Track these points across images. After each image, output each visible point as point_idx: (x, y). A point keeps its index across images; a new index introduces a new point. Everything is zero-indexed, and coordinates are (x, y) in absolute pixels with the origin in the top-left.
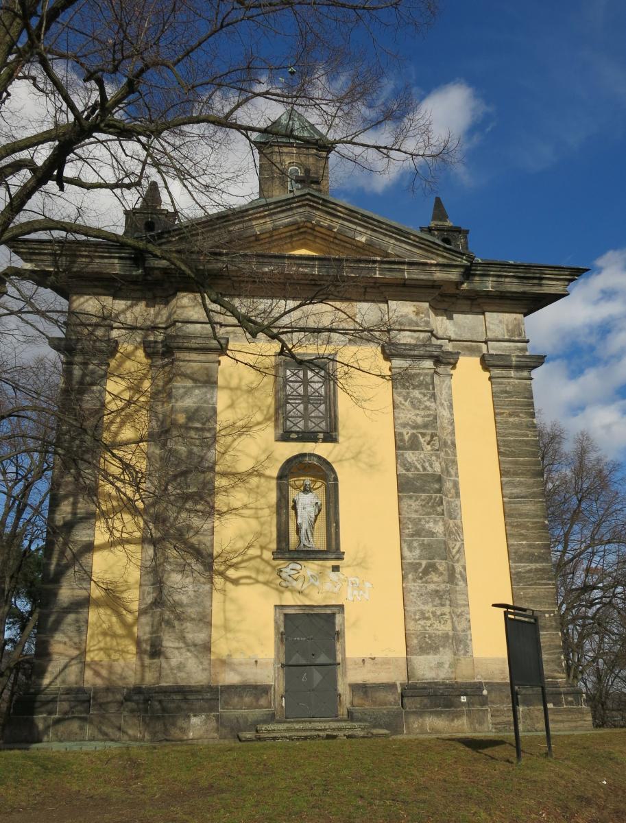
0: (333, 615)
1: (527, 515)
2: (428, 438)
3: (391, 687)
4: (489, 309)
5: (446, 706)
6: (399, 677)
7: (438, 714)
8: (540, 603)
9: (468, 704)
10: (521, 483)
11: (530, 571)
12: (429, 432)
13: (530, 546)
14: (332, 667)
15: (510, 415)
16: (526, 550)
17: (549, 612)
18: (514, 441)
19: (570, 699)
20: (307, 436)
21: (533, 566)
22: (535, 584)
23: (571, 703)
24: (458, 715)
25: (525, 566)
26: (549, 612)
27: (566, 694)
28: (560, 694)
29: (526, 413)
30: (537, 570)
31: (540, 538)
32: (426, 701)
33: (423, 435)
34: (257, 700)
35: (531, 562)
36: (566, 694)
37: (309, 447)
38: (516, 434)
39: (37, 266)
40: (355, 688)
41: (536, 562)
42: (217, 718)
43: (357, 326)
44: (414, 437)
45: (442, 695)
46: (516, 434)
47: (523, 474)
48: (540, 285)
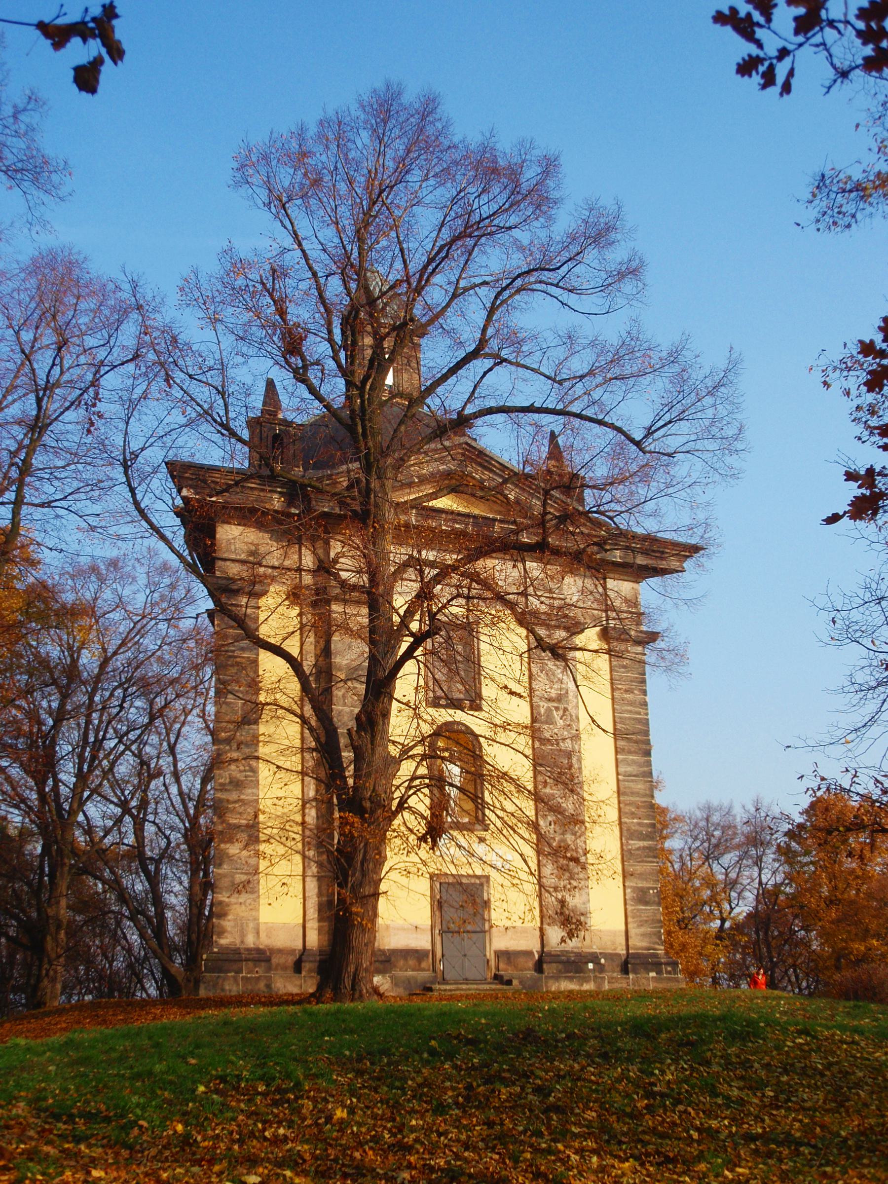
0: (482, 885)
1: (637, 794)
2: (561, 713)
3: (529, 953)
4: (612, 575)
5: (576, 972)
6: (534, 946)
7: (571, 979)
8: (646, 880)
9: (594, 970)
10: (634, 762)
11: (638, 849)
12: (562, 706)
13: (639, 824)
14: (483, 931)
15: (626, 691)
16: (637, 828)
17: (653, 888)
18: (630, 718)
19: (669, 969)
20: (455, 704)
21: (642, 844)
22: (642, 861)
23: (669, 972)
24: (587, 980)
25: (636, 844)
26: (653, 888)
27: (667, 964)
28: (661, 964)
29: (640, 690)
30: (644, 848)
31: (648, 817)
32: (560, 966)
33: (557, 709)
34: (420, 963)
35: (640, 840)
36: (667, 964)
37: (459, 716)
38: (630, 712)
39: (196, 494)
40: (499, 954)
41: (644, 840)
42: (391, 977)
43: (224, 419)
44: (549, 710)
45: (574, 962)
46: (630, 712)
47: (635, 753)
48: (662, 559)
